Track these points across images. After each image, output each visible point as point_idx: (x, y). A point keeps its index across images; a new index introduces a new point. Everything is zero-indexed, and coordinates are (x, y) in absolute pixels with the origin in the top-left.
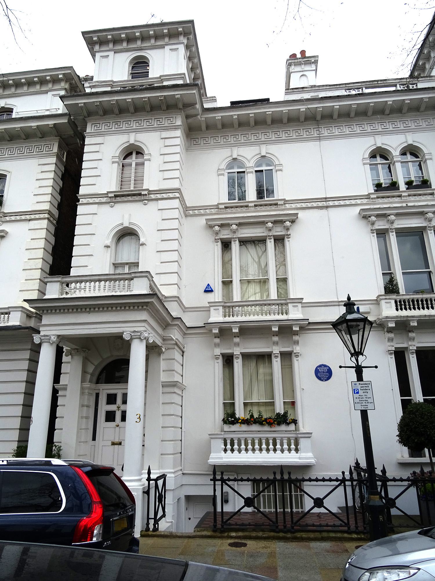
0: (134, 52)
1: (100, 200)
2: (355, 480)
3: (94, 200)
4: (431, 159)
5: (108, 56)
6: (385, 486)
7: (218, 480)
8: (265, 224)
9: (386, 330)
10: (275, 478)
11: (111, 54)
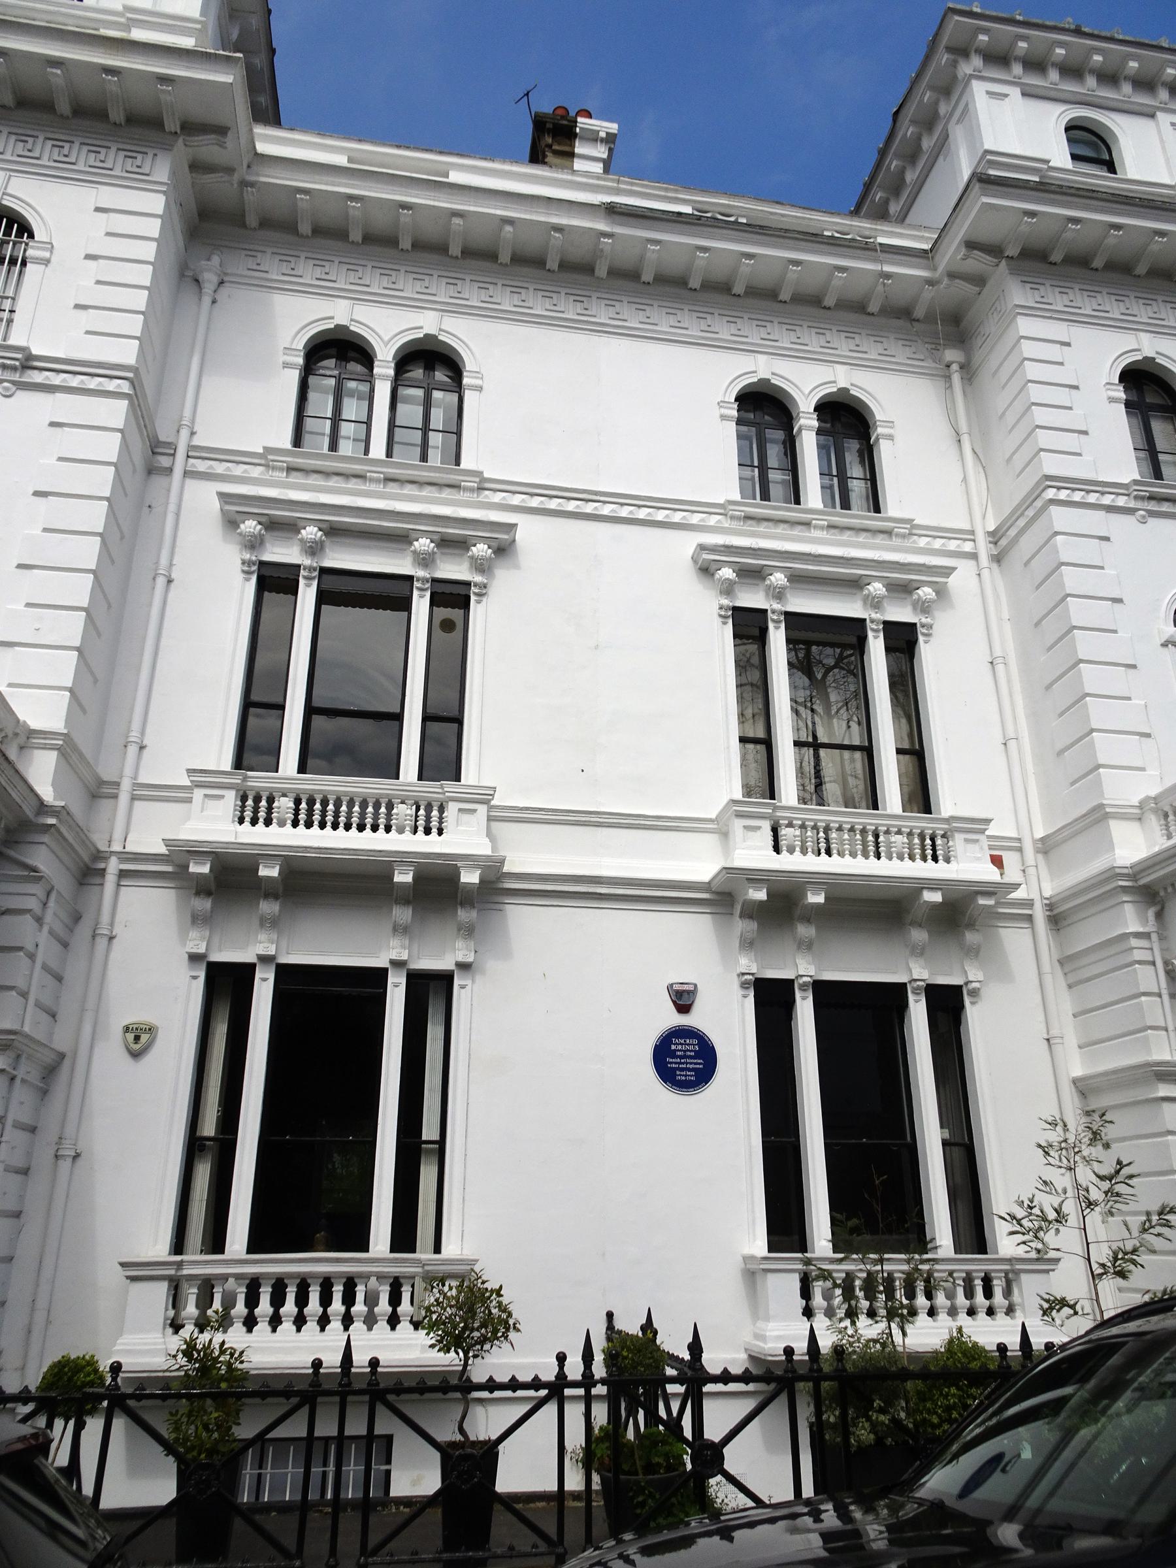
1: (82, 382)
2: (827, 1378)
3: (64, 380)
4: (479, 389)
5: (1006, 96)
6: (695, 1397)
9: (738, 909)
10: (561, 1375)
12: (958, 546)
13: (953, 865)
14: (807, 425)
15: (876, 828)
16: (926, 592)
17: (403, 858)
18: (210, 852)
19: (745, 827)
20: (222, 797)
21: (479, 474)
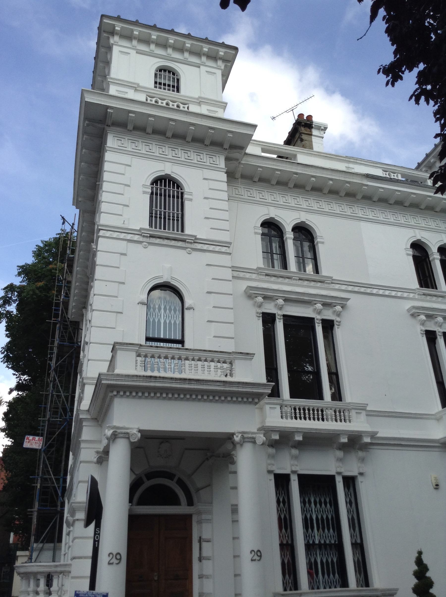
0: (162, 60)
3: (104, 233)
8: (312, 305)
11: (133, 52)
12: (346, 288)
13: (352, 424)
14: (289, 236)
15: (335, 409)
16: (338, 308)
17: (344, 432)
18: (279, 431)
19: (356, 413)
20: (276, 408)
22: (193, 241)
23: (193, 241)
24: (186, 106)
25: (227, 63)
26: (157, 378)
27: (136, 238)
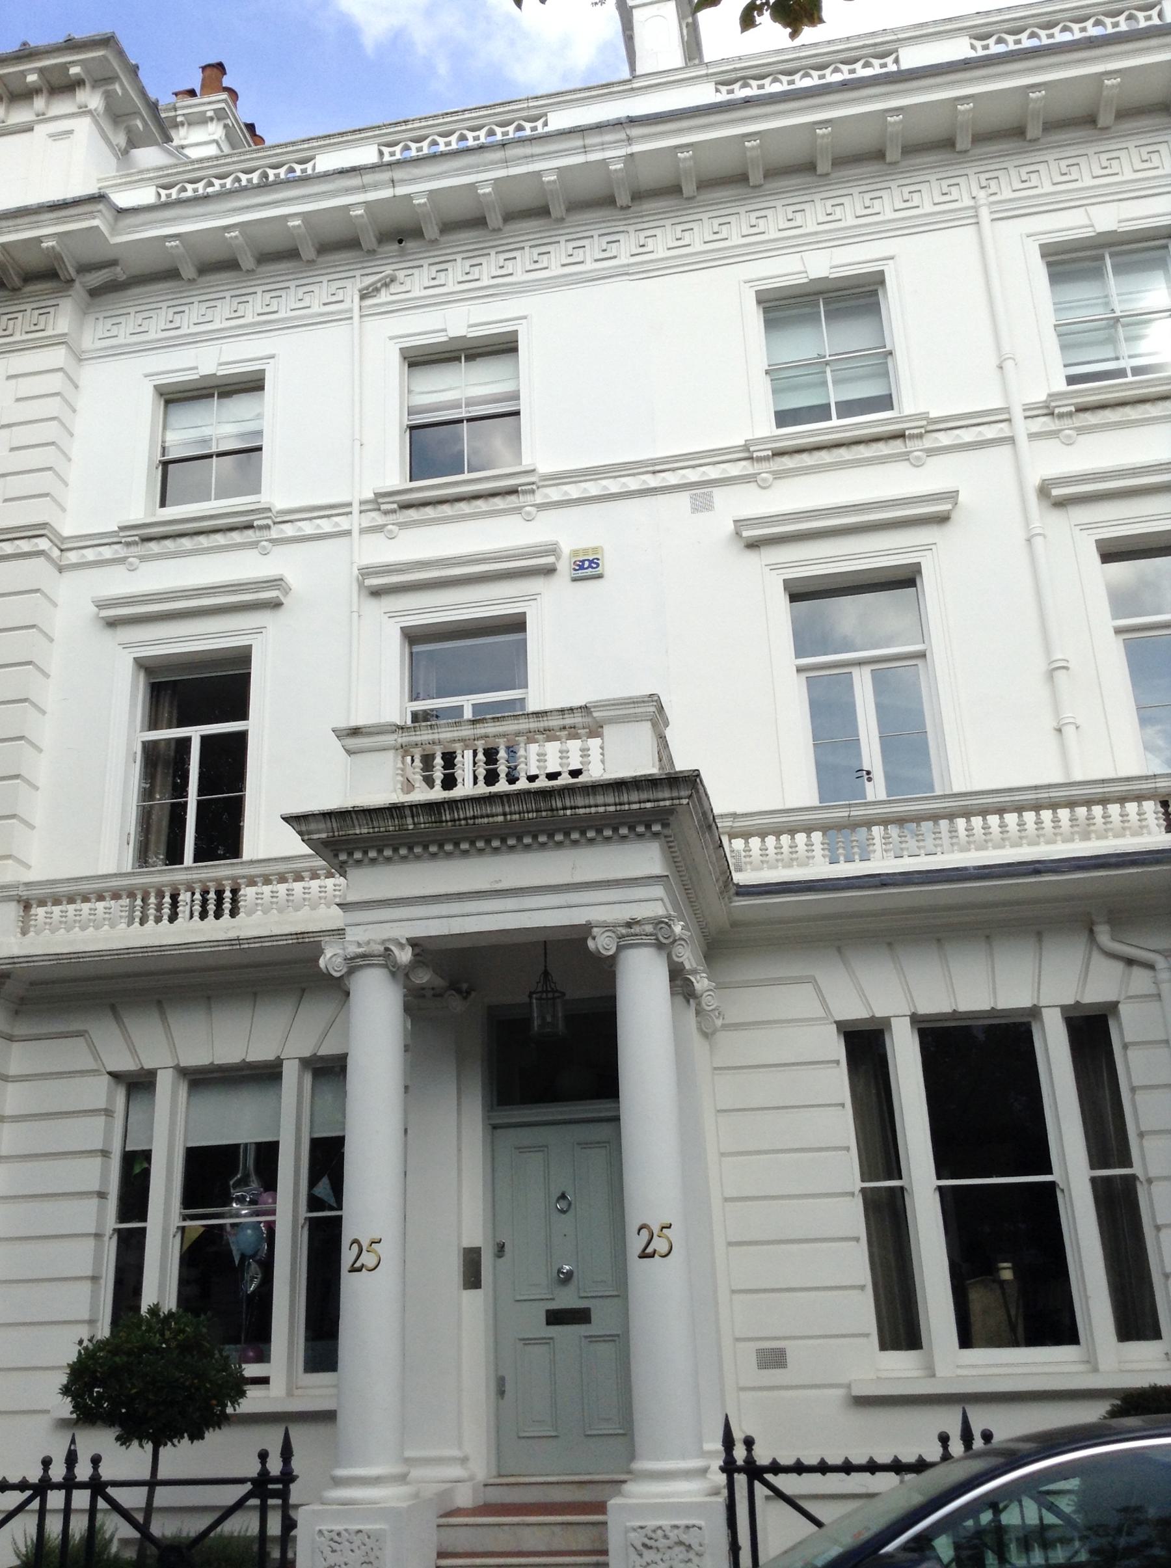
7: (82, 1486)
10: (264, 1472)
21: (924, 416)
22: (923, 430)
23: (923, 430)
24: (1154, 13)
25: (107, 84)
26: (878, 883)
27: (734, 470)
